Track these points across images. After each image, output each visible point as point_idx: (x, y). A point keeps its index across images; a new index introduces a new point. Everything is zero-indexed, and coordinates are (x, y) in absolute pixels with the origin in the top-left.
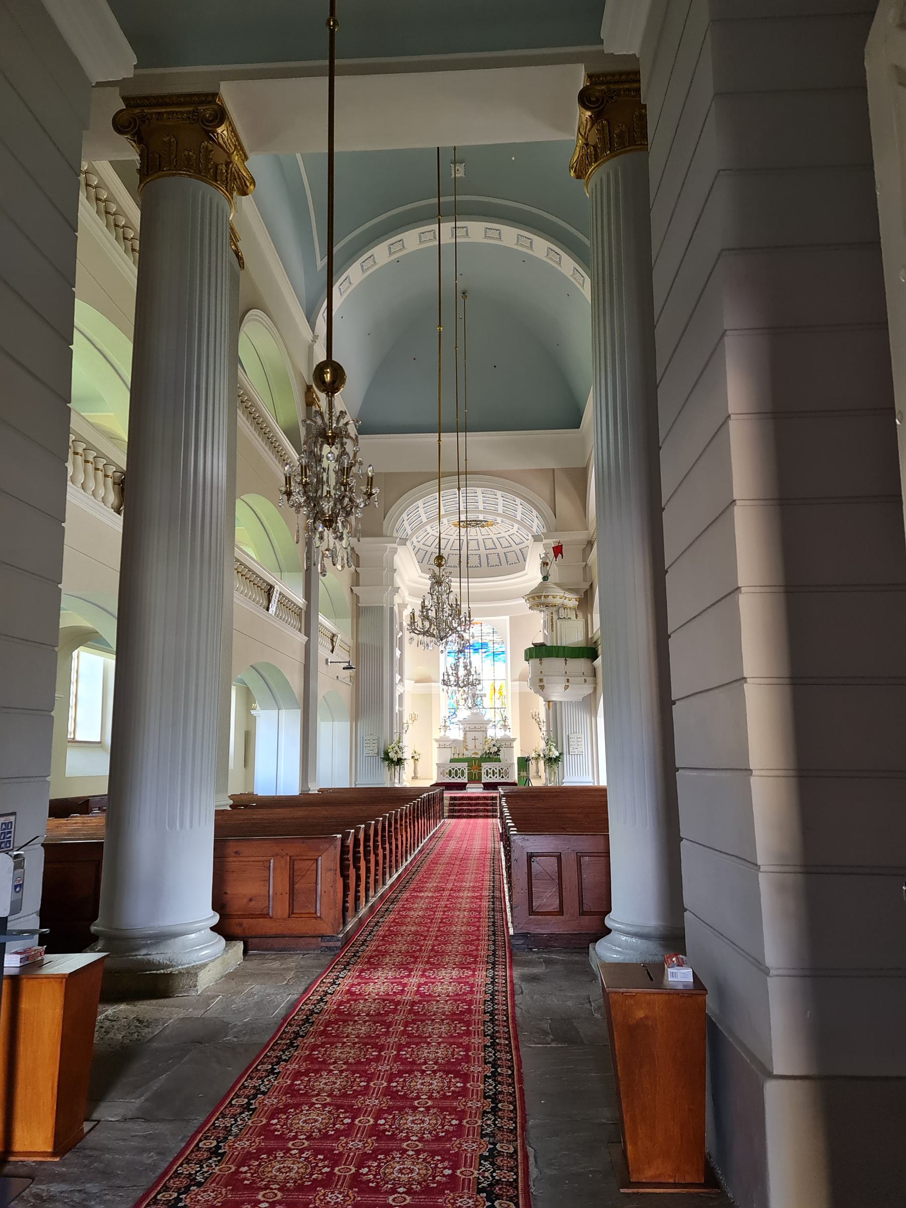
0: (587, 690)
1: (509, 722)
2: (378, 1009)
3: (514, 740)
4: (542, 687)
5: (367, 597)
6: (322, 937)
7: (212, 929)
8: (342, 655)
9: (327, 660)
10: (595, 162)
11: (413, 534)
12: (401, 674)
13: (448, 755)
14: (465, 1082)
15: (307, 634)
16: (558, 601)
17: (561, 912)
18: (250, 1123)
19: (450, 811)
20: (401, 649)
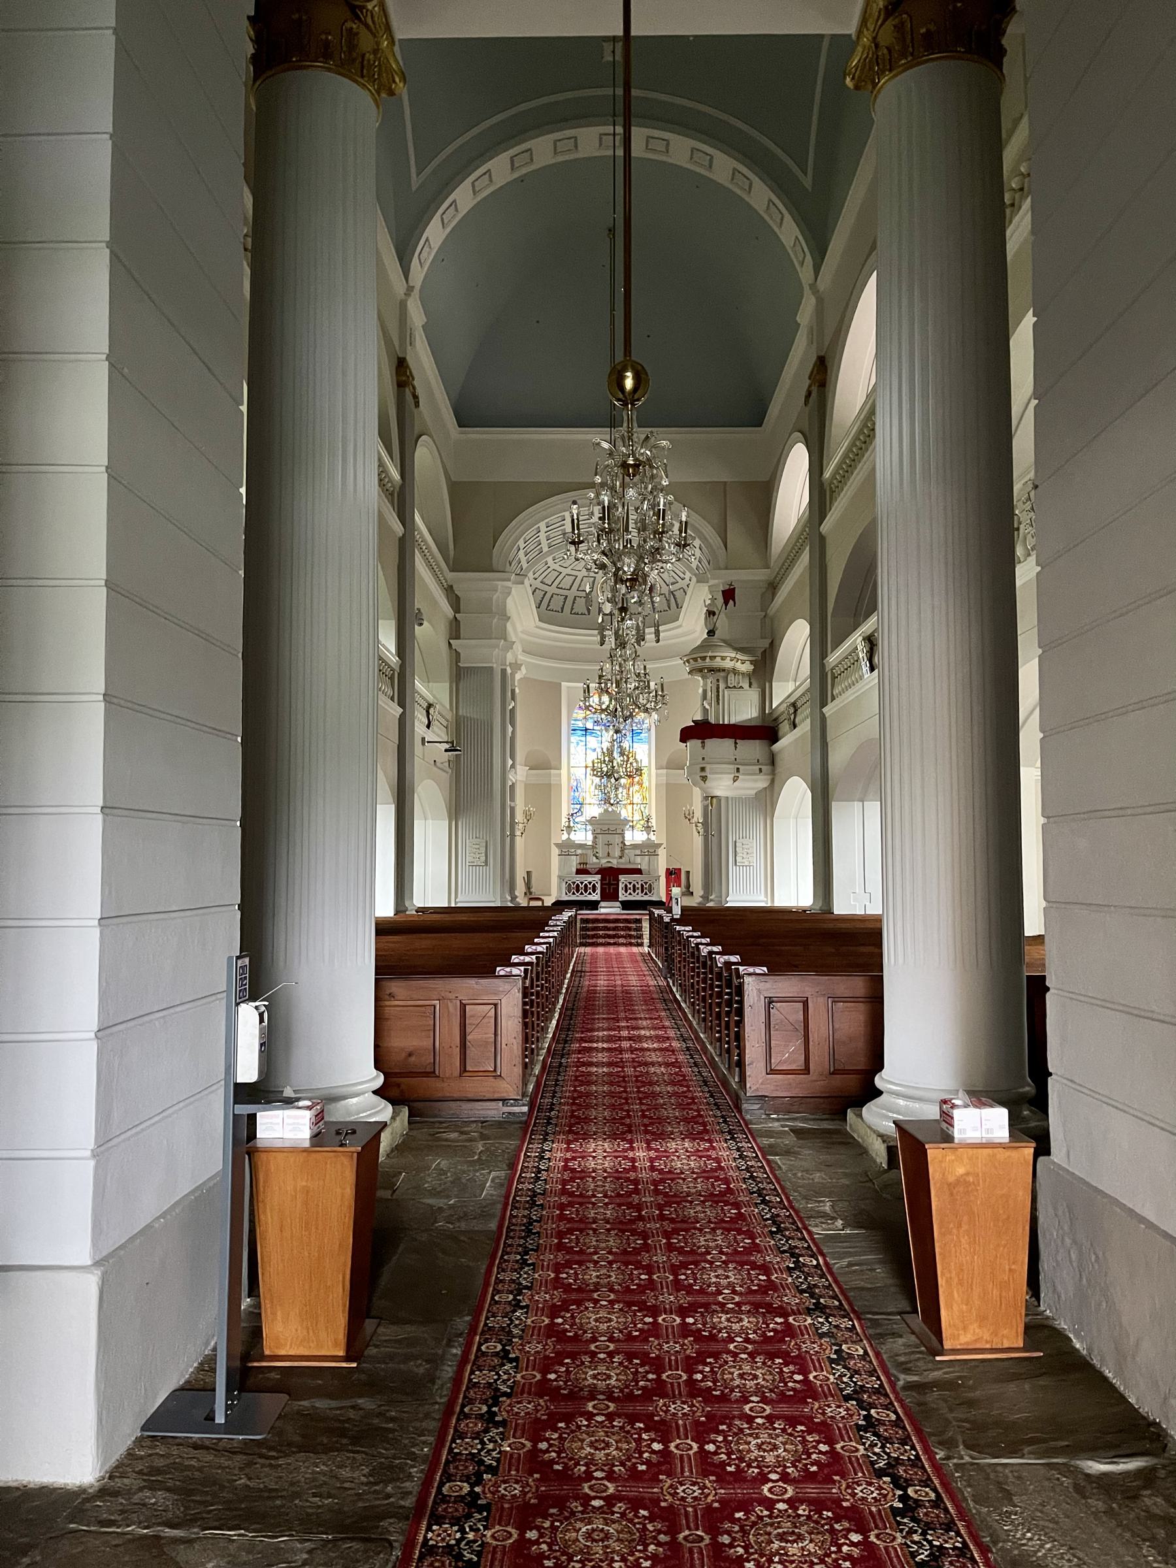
0: (761, 782)
1: (653, 822)
2: (616, 1189)
3: (660, 845)
4: (704, 779)
5: (473, 651)
6: (504, 1101)
7: (375, 1092)
8: (438, 733)
9: (423, 739)
10: (890, 70)
11: (528, 570)
12: (513, 757)
13: (574, 863)
14: (650, 1273)
15: (402, 704)
16: (728, 664)
17: (806, 1070)
18: (529, 1321)
19: (583, 937)
20: (513, 726)
